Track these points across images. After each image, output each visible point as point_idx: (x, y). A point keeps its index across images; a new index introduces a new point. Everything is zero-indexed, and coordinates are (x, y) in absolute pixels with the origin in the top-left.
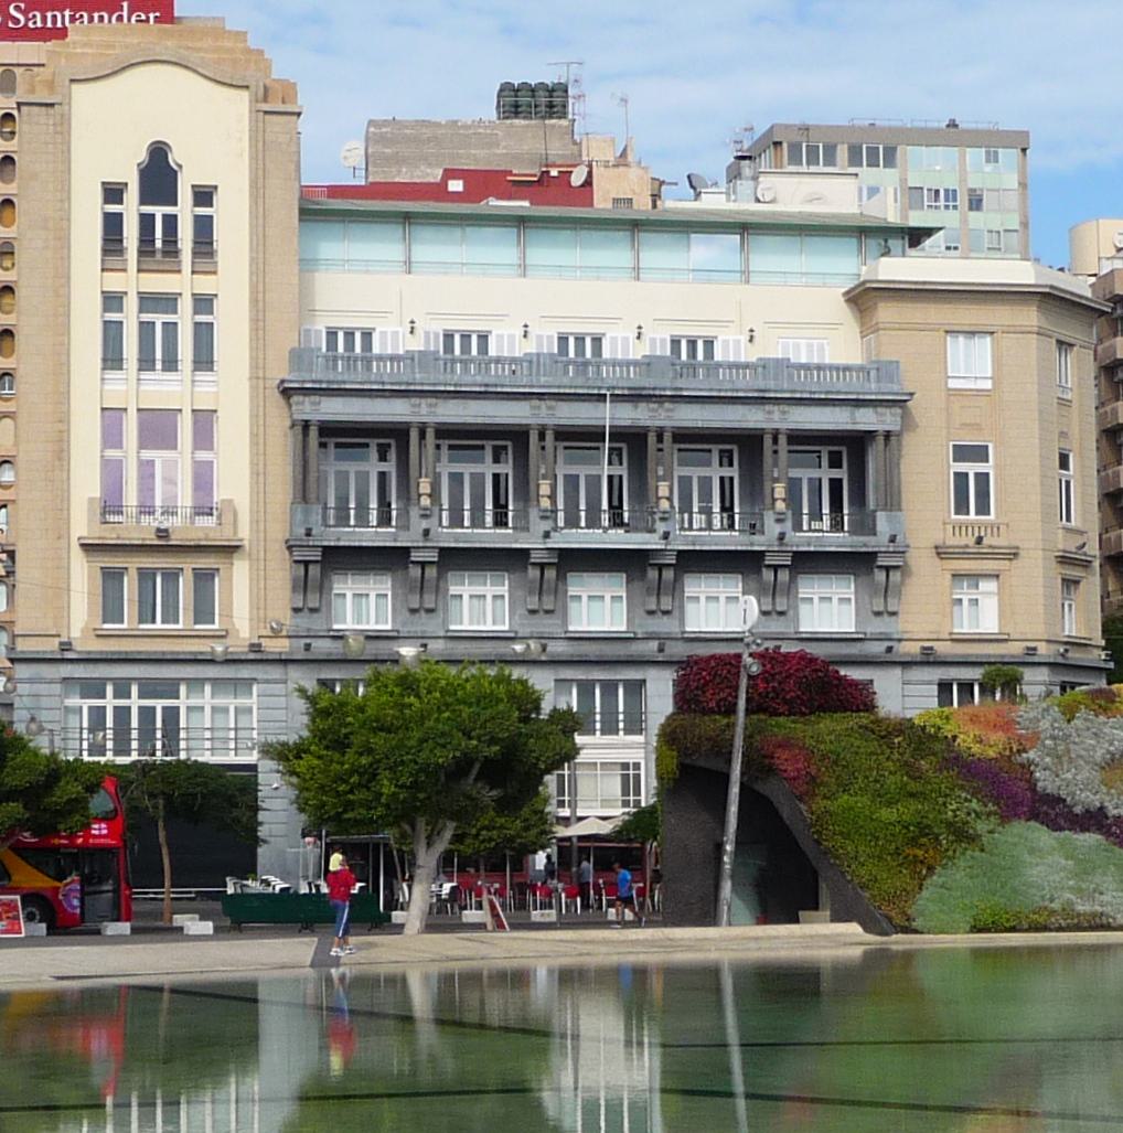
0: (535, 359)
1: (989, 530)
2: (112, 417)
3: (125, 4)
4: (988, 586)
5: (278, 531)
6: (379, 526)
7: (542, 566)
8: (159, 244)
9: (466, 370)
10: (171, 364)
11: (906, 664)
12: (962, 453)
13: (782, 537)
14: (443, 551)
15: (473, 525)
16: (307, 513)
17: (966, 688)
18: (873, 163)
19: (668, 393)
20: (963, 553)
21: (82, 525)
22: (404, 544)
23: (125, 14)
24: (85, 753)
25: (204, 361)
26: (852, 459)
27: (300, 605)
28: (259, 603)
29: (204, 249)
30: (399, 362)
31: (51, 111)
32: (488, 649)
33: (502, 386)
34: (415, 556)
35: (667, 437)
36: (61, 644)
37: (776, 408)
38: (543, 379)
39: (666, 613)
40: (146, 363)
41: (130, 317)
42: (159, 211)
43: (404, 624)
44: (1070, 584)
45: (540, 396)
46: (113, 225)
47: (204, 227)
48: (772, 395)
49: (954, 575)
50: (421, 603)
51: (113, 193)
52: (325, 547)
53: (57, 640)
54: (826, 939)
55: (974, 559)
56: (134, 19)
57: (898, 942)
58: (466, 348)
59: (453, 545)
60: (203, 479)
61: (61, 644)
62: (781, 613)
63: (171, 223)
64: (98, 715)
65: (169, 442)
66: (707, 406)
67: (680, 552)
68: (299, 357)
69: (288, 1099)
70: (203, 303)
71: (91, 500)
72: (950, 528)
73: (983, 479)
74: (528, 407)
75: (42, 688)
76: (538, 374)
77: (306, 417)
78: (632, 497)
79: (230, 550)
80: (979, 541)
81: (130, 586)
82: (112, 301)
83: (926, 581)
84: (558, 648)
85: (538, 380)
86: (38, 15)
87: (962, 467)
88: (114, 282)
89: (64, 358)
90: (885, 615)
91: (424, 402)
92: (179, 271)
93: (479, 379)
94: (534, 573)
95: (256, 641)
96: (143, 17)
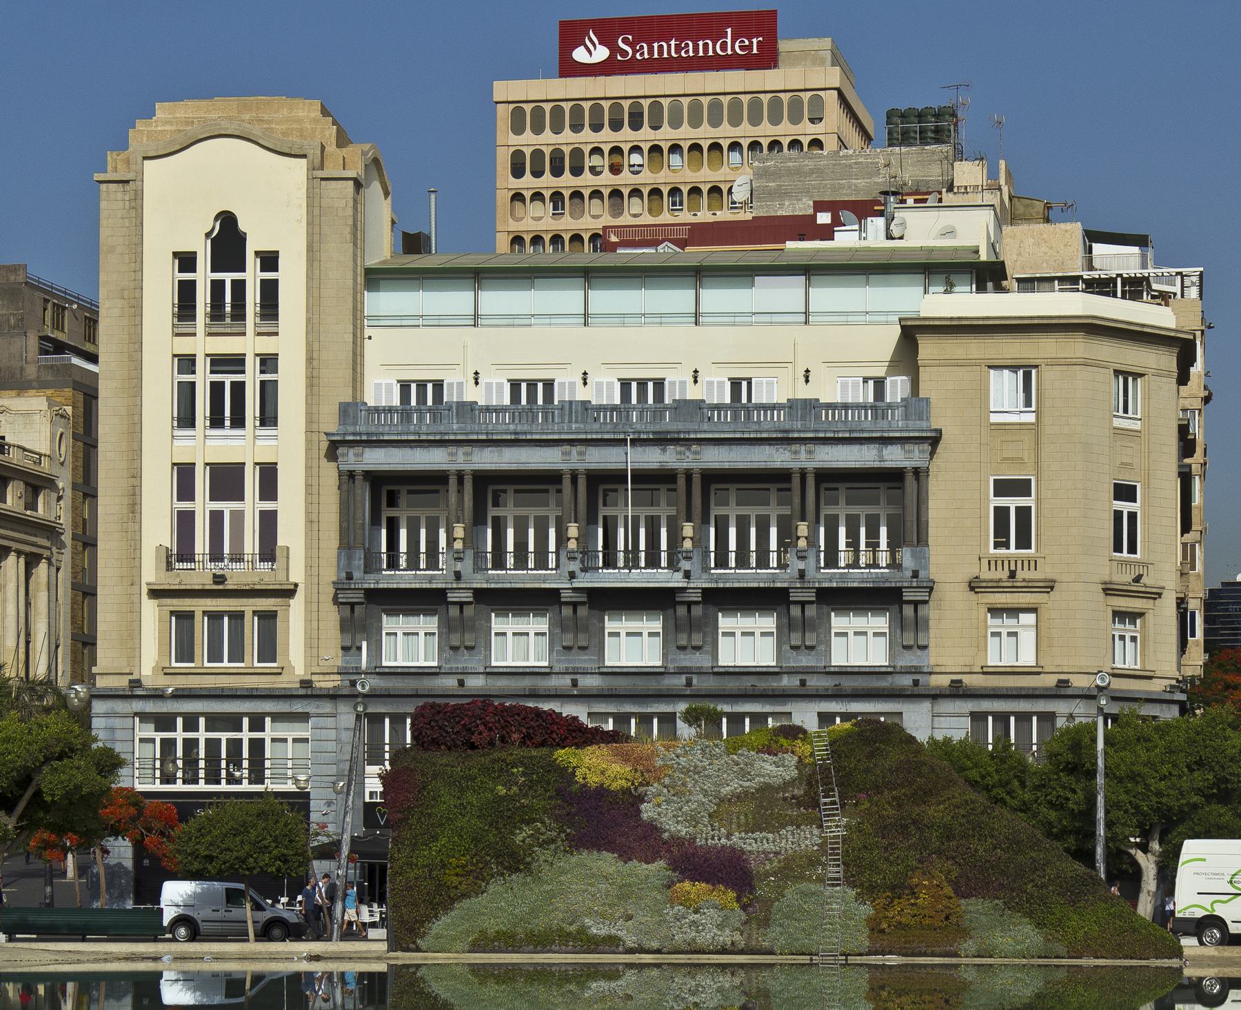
1: (1019, 563)
2: (185, 473)
3: (729, 30)
4: (1028, 619)
5: (330, 574)
6: (736, 568)
7: (575, 605)
8: (228, 309)
9: (421, 419)
10: (238, 422)
11: (936, 696)
12: (1003, 488)
13: (802, 574)
15: (759, 566)
16: (350, 558)
20: (996, 586)
21: (151, 573)
22: (440, 586)
23: (729, 41)
24: (137, 781)
25: (268, 418)
26: (892, 494)
27: (349, 644)
28: (312, 643)
30: (612, 412)
31: (128, 187)
32: (526, 683)
33: (532, 433)
34: (452, 597)
35: (697, 480)
36: (131, 681)
37: (803, 448)
39: (697, 648)
40: (216, 421)
41: (203, 378)
42: (228, 277)
43: (448, 661)
45: (571, 442)
46: (187, 292)
47: (270, 291)
50: (804, 640)
51: (186, 261)
52: (475, 589)
55: (1006, 594)
56: (737, 44)
59: (485, 586)
61: (131, 681)
62: (812, 648)
63: (239, 287)
64: (168, 745)
65: (237, 494)
66: (734, 447)
67: (705, 590)
68: (348, 411)
70: (268, 362)
72: (985, 562)
73: (1024, 513)
74: (445, 454)
75: (118, 722)
76: (570, 421)
77: (350, 468)
80: (1012, 575)
81: (202, 627)
82: (187, 363)
84: (590, 682)
85: (570, 428)
86: (691, 44)
87: (1003, 501)
88: (185, 346)
89: (136, 417)
90: (689, 650)
91: (461, 450)
92: (244, 334)
93: (512, 427)
94: (567, 611)
95: (308, 677)
96: (747, 43)
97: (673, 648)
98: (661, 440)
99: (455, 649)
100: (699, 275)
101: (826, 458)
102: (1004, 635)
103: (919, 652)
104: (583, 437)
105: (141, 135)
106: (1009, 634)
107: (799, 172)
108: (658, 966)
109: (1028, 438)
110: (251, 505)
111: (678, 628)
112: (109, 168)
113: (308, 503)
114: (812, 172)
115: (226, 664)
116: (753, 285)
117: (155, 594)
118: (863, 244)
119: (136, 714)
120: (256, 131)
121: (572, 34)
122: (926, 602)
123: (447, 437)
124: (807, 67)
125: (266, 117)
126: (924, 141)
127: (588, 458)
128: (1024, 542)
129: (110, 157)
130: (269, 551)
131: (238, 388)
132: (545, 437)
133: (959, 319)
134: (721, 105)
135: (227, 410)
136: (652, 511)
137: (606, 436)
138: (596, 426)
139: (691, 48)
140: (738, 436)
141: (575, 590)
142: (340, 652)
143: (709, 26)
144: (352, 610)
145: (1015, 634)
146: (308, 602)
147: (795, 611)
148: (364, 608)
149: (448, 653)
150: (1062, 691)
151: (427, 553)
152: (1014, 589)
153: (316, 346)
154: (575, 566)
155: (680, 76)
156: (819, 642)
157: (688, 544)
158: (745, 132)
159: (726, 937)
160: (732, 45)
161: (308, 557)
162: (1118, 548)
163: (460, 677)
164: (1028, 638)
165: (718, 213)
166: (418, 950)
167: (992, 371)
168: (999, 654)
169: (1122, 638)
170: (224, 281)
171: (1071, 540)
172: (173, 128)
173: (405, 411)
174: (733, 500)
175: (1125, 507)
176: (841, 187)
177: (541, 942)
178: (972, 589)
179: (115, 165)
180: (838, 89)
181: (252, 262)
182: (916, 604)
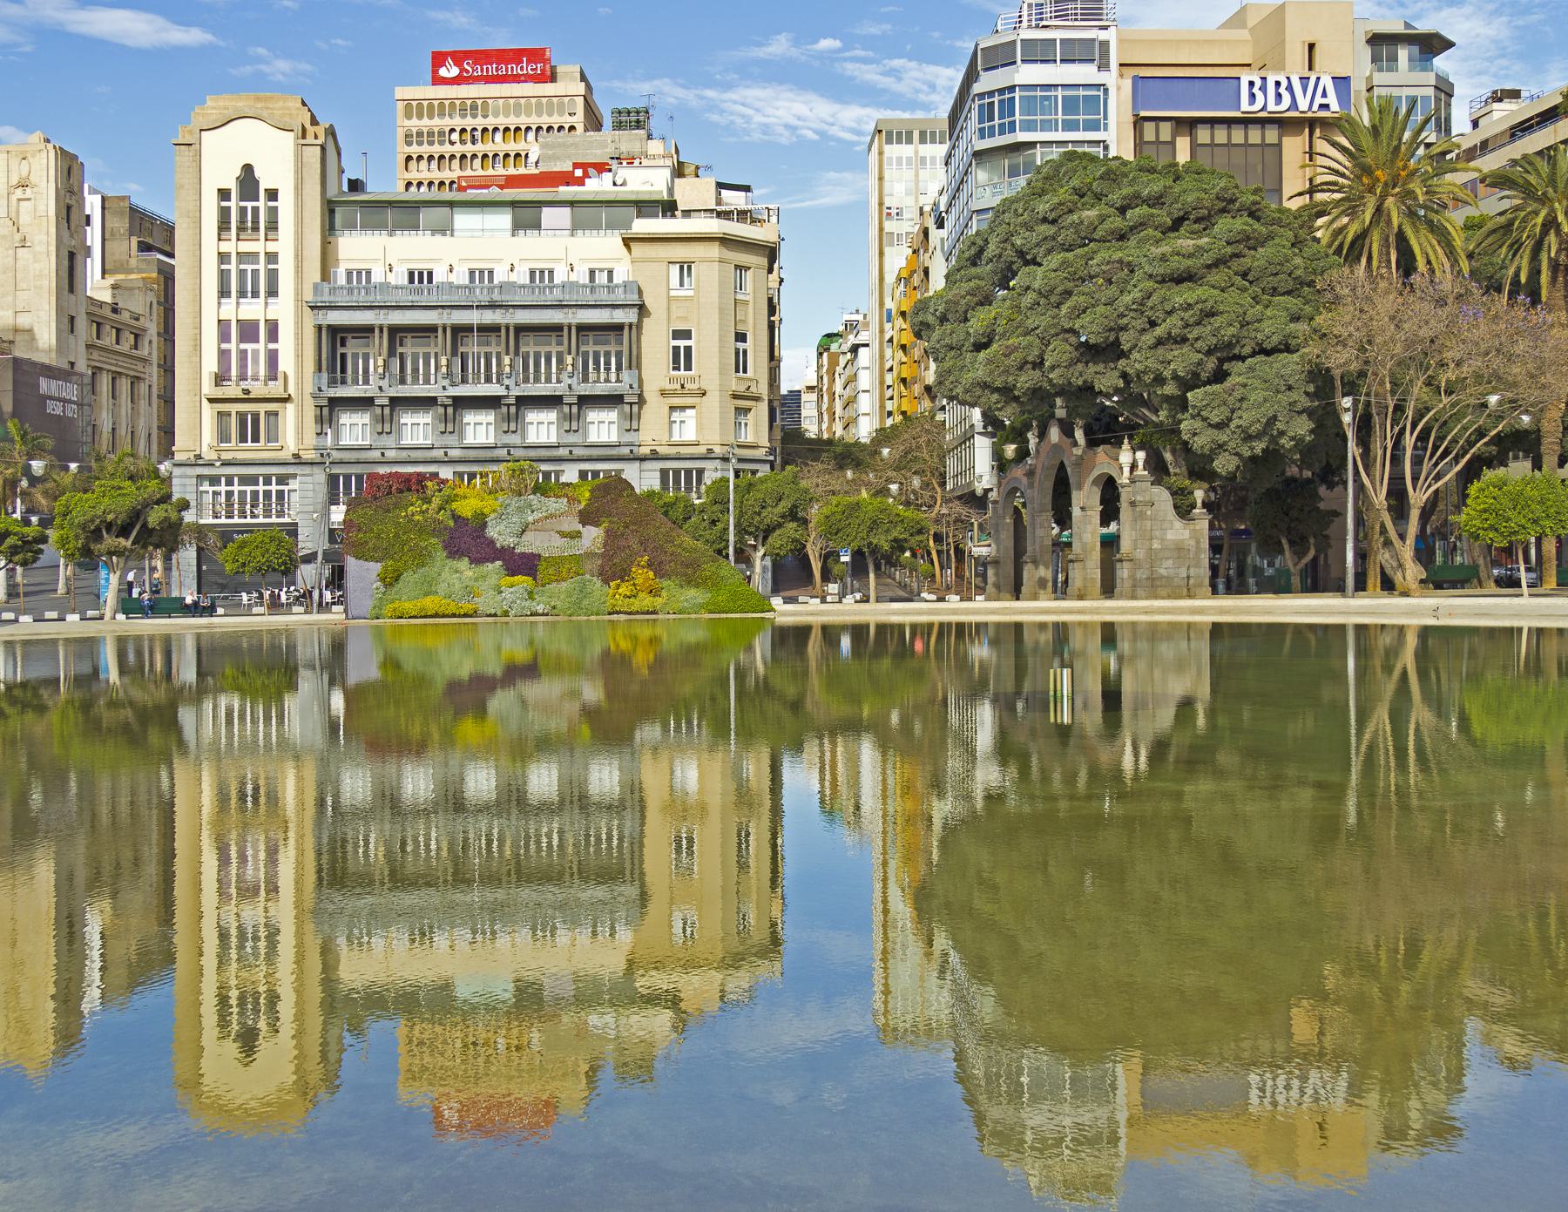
2: (223, 325)
5: (309, 388)
10: (255, 294)
11: (643, 459)
12: (677, 334)
14: (580, 397)
18: (899, 142)
25: (272, 292)
34: (377, 402)
40: (242, 294)
42: (249, 205)
44: (742, 411)
45: (443, 307)
47: (273, 212)
51: (224, 194)
55: (680, 399)
70: (272, 257)
73: (688, 349)
75: (188, 481)
82: (223, 257)
83: (655, 409)
88: (225, 247)
121: (439, 59)
126: (631, 128)
130: (272, 374)
136: (426, 350)
152: (683, 395)
175: (741, 345)
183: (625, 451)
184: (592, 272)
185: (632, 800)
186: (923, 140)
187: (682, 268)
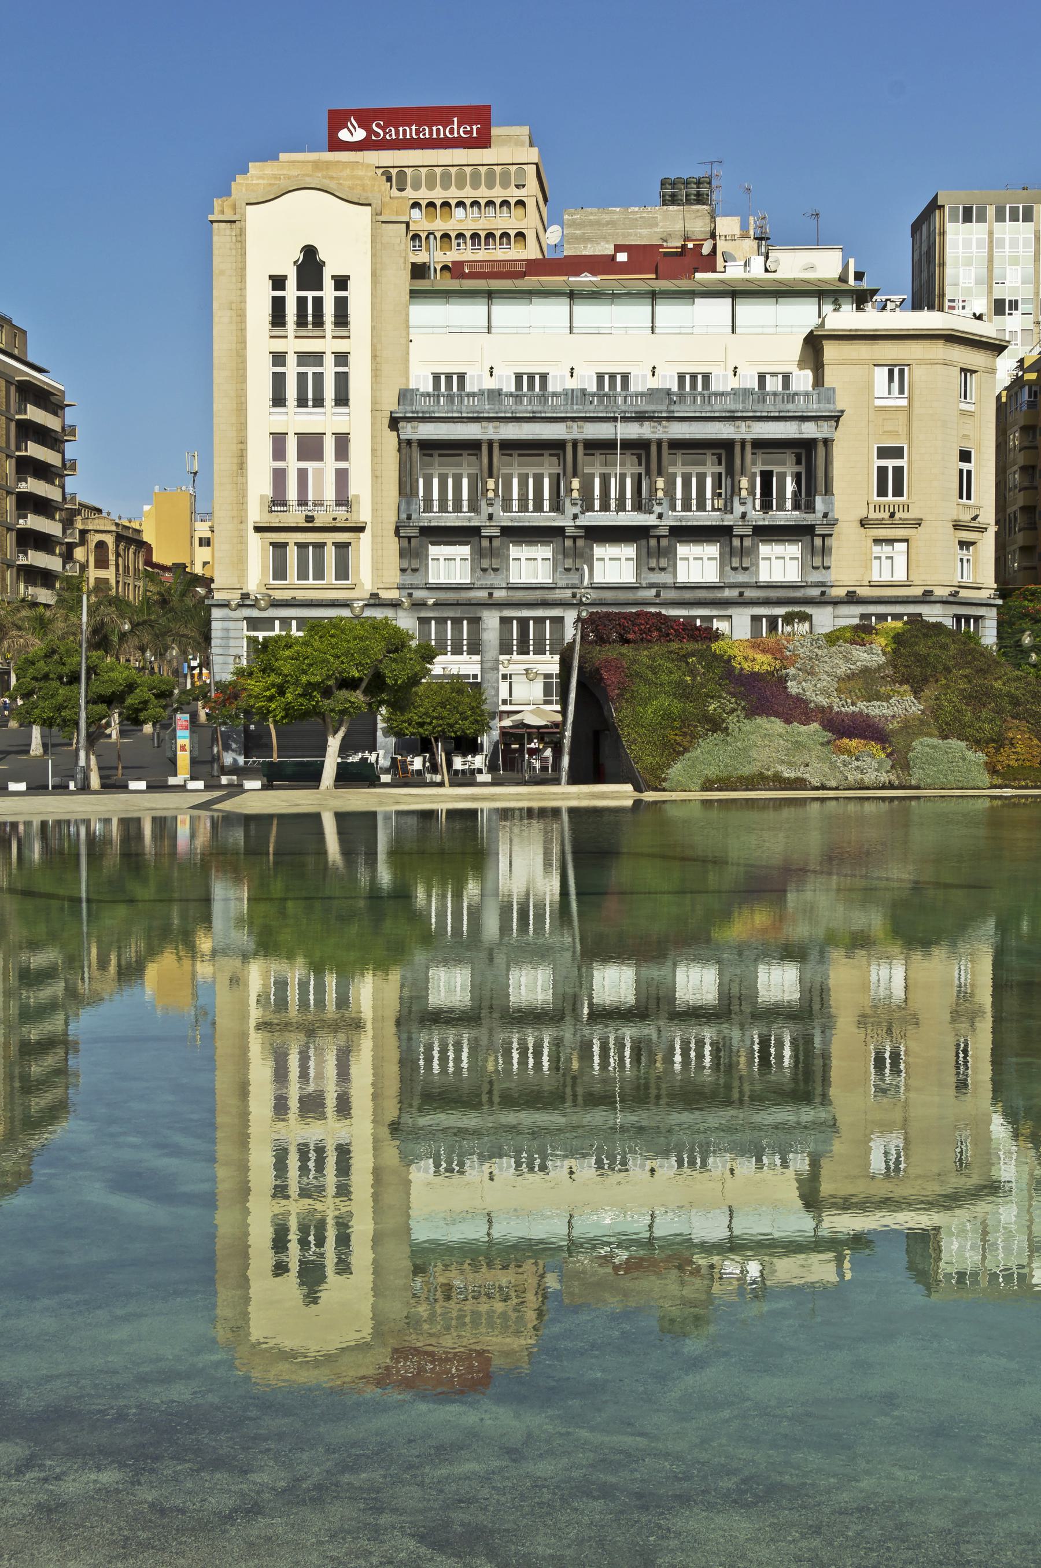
0: (570, 393)
2: (279, 440)
3: (455, 119)
4: (901, 547)
5: (391, 517)
7: (574, 538)
8: (310, 319)
10: (319, 402)
11: (836, 603)
12: (884, 453)
17: (773, 621)
19: (664, 415)
21: (256, 514)
23: (455, 127)
25: (342, 400)
26: (809, 458)
28: (377, 567)
29: (341, 320)
30: (637, 397)
31: (234, 226)
34: (485, 532)
35: (665, 445)
36: (242, 594)
38: (575, 407)
39: (663, 569)
40: (302, 402)
41: (291, 370)
42: (310, 295)
43: (479, 579)
45: (573, 419)
46: (278, 305)
47: (342, 305)
48: (740, 414)
49: (874, 541)
51: (278, 282)
53: (240, 591)
54: (618, 795)
55: (888, 527)
57: (649, 796)
58: (694, 386)
59: (510, 524)
60: (342, 477)
61: (242, 594)
62: (746, 569)
63: (318, 302)
65: (319, 456)
68: (405, 395)
69: (365, 898)
70: (342, 358)
71: (262, 497)
73: (898, 471)
75: (231, 625)
76: (572, 404)
78: (727, 491)
79: (361, 529)
80: (892, 515)
81: (292, 554)
82: (279, 358)
84: (500, 594)
87: (883, 463)
88: (279, 346)
93: (529, 408)
97: (645, 569)
98: (641, 418)
99: (484, 570)
100: (490, 295)
101: (760, 431)
102: (523, 560)
103: (824, 571)
104: (583, 415)
105: (241, 187)
106: (887, 558)
107: (598, 223)
108: (837, 799)
109: (902, 417)
110: (330, 462)
111: (649, 555)
112: (216, 211)
113: (374, 463)
114: (608, 223)
115: (311, 581)
116: (531, 303)
117: (258, 529)
118: (747, 276)
119: (245, 618)
120: (332, 186)
121: (338, 119)
122: (831, 535)
123: (482, 415)
124: (512, 147)
125: (334, 175)
126: (689, 202)
127: (585, 431)
128: (898, 492)
129: (217, 203)
130: (343, 500)
131: (319, 378)
132: (555, 415)
133: (856, 330)
134: (450, 175)
135: (310, 397)
136: (538, 470)
137: (600, 415)
138: (591, 408)
139: (393, 132)
140: (697, 414)
141: (576, 527)
142: (398, 572)
143: (440, 115)
144: (409, 542)
145: (891, 558)
146: (374, 536)
147: (736, 542)
148: (416, 539)
149: (479, 573)
150: (927, 598)
151: (534, 500)
152: (894, 526)
153: (379, 347)
154: (576, 510)
155: (419, 152)
156: (752, 565)
157: (660, 494)
158: (468, 194)
159: (884, 778)
160: (457, 130)
161: (374, 502)
162: (961, 497)
163: (491, 591)
164: (901, 561)
165: (448, 253)
166: (664, 790)
167: (876, 368)
168: (882, 573)
169: (962, 560)
170: (306, 298)
171: (930, 491)
172: (265, 182)
173: (517, 397)
174: (679, 463)
175: (965, 466)
176: (629, 235)
177: (750, 783)
178: (862, 525)
179: (220, 208)
180: (536, 164)
181: (328, 284)
182: (824, 536)
183: (815, 592)
184: (762, 378)
185: (810, 1011)
186: (1000, 217)
187: (891, 373)
